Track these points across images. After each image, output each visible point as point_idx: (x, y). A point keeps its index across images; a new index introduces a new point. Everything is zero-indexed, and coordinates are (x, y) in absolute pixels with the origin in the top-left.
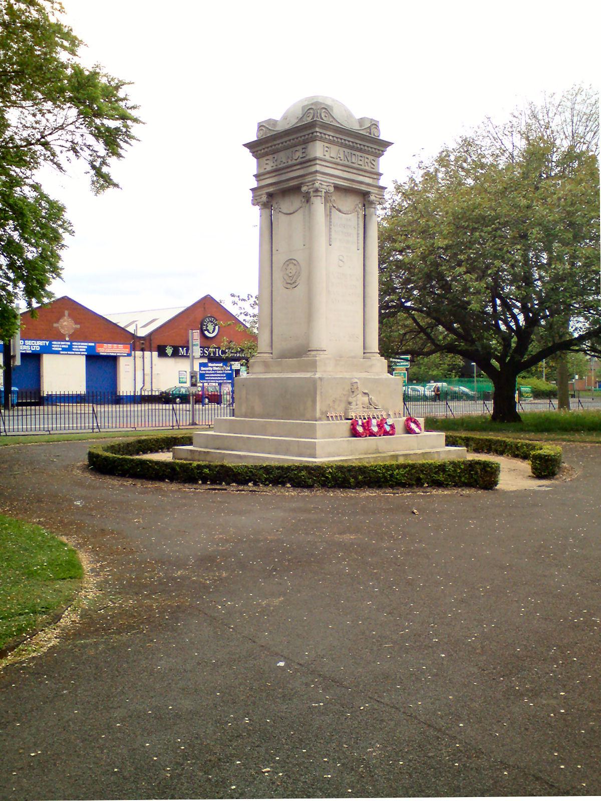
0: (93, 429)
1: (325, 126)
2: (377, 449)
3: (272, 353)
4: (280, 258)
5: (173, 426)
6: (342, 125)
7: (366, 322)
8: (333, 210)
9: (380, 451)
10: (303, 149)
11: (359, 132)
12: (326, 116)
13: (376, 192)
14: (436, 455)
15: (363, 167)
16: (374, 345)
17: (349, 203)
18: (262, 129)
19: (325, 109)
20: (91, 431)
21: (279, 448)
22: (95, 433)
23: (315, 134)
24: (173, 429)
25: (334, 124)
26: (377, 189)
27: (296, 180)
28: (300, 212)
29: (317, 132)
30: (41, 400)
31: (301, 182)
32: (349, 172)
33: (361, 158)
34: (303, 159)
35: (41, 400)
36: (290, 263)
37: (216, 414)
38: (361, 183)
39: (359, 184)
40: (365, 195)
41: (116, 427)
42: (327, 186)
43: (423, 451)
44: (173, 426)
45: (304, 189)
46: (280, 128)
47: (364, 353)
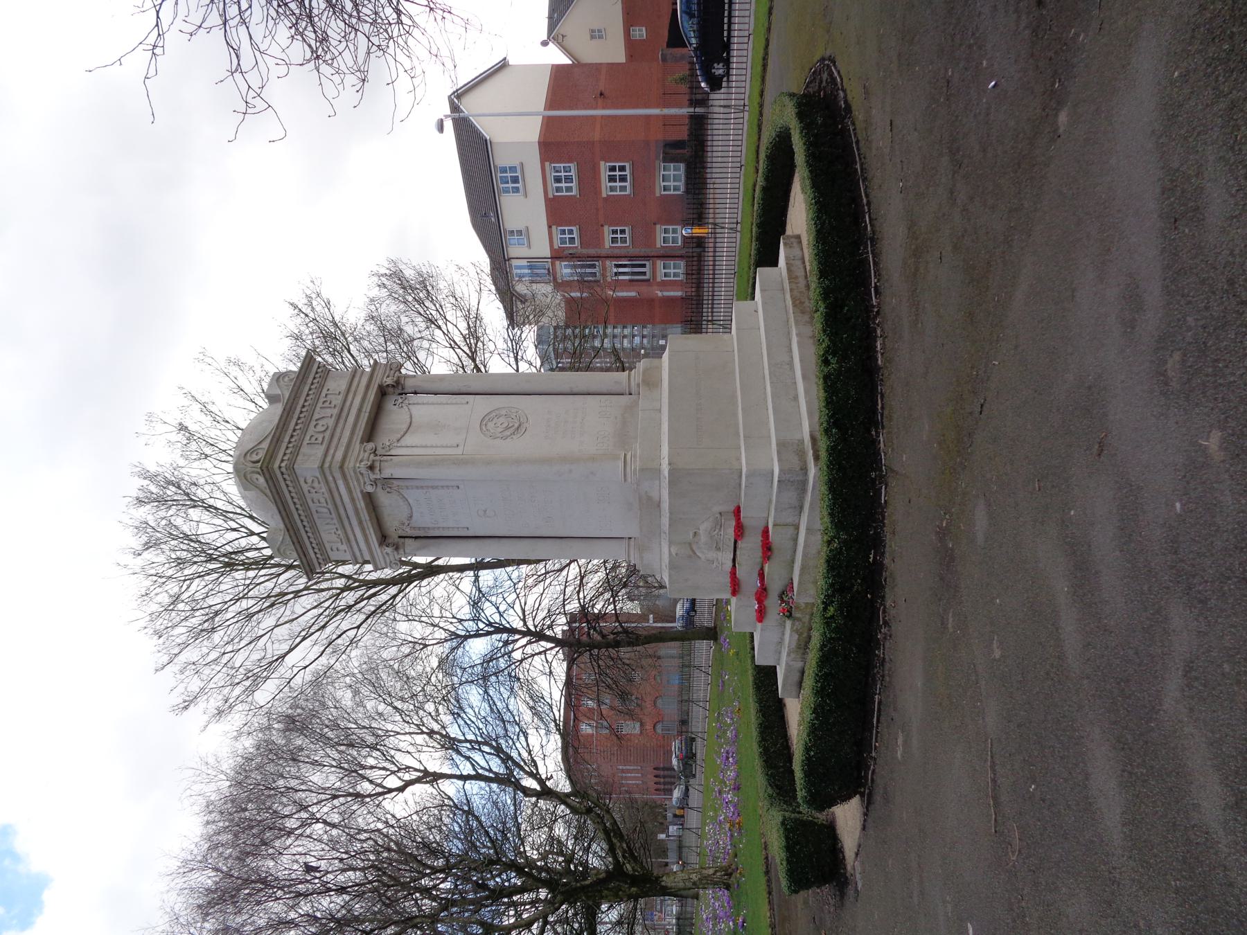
0: (737, 223)
1: (271, 454)
6: (270, 433)
7: (584, 540)
8: (410, 407)
10: (313, 502)
11: (270, 494)
12: (257, 454)
15: (330, 506)
17: (396, 415)
18: (284, 550)
21: (781, 370)
23: (283, 470)
25: (265, 445)
29: (280, 467)
30: (715, 627)
33: (313, 439)
35: (715, 627)
37: (724, 143)
38: (360, 410)
39: (367, 401)
40: (383, 392)
41: (739, 178)
44: (737, 223)
45: (370, 489)
46: (277, 522)
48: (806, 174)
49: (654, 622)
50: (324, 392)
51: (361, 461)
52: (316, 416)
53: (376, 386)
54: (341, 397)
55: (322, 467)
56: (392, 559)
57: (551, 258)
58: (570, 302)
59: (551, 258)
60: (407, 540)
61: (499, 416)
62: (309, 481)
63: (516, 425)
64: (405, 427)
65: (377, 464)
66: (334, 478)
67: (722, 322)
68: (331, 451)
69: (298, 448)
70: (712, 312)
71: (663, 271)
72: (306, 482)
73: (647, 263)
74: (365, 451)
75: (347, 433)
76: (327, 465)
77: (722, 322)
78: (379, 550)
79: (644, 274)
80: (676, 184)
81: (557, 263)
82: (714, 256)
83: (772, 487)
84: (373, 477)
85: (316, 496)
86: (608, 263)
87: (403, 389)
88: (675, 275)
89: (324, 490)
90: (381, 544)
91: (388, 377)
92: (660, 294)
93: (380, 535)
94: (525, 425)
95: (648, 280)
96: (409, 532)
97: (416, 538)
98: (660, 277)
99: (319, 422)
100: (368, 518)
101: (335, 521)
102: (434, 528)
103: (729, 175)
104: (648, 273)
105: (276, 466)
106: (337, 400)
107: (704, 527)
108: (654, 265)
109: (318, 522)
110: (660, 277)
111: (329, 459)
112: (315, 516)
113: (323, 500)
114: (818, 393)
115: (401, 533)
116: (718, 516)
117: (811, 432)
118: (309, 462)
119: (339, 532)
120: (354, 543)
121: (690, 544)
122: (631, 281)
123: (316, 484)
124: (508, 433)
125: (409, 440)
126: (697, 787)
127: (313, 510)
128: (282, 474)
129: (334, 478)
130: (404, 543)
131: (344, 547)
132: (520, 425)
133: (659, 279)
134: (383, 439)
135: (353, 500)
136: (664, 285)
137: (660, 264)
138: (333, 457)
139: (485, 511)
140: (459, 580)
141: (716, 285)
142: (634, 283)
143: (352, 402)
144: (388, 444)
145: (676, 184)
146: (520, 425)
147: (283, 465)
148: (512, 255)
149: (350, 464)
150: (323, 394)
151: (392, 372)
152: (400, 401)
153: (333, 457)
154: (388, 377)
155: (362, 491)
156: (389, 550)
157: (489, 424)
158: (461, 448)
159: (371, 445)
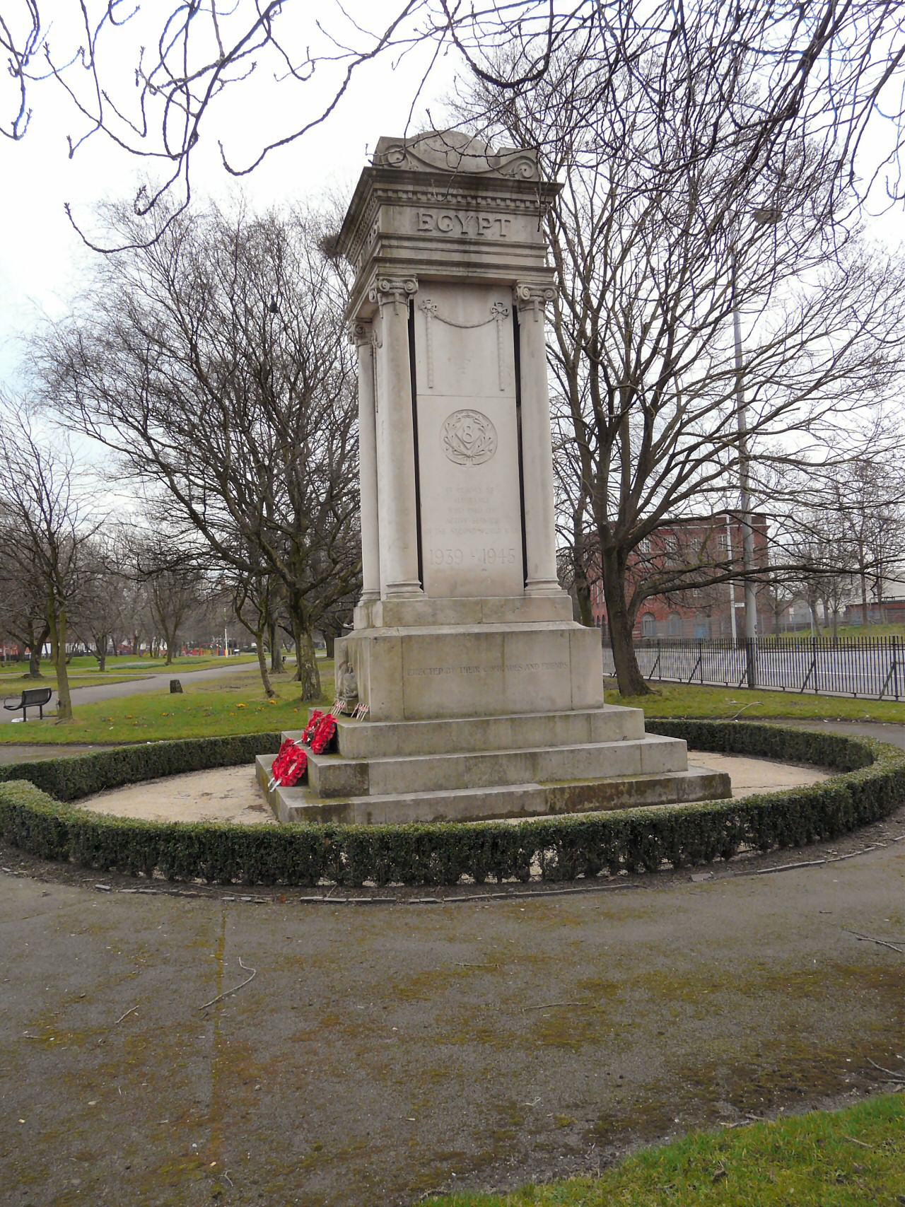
0: (897, 697)
4: (433, 412)
24: (897, 701)
36: (468, 416)
47: (526, 585)
48: (40, 810)
49: (387, 625)
50: (503, 217)
53: (513, 277)
54: (496, 238)
61: (482, 429)
63: (469, 453)
64: (461, 321)
65: (391, 299)
68: (406, 244)
74: (405, 282)
75: (437, 256)
83: (447, 752)
91: (530, 289)
94: (469, 463)
106: (490, 235)
111: (394, 243)
114: (34, 761)
124: (455, 443)
125: (438, 330)
132: (469, 457)
134: (428, 299)
138: (398, 247)
140: (778, 518)
143: (507, 254)
144: (429, 306)
146: (469, 457)
151: (540, 293)
153: (398, 247)
154: (530, 289)
158: (429, 392)
159: (414, 286)
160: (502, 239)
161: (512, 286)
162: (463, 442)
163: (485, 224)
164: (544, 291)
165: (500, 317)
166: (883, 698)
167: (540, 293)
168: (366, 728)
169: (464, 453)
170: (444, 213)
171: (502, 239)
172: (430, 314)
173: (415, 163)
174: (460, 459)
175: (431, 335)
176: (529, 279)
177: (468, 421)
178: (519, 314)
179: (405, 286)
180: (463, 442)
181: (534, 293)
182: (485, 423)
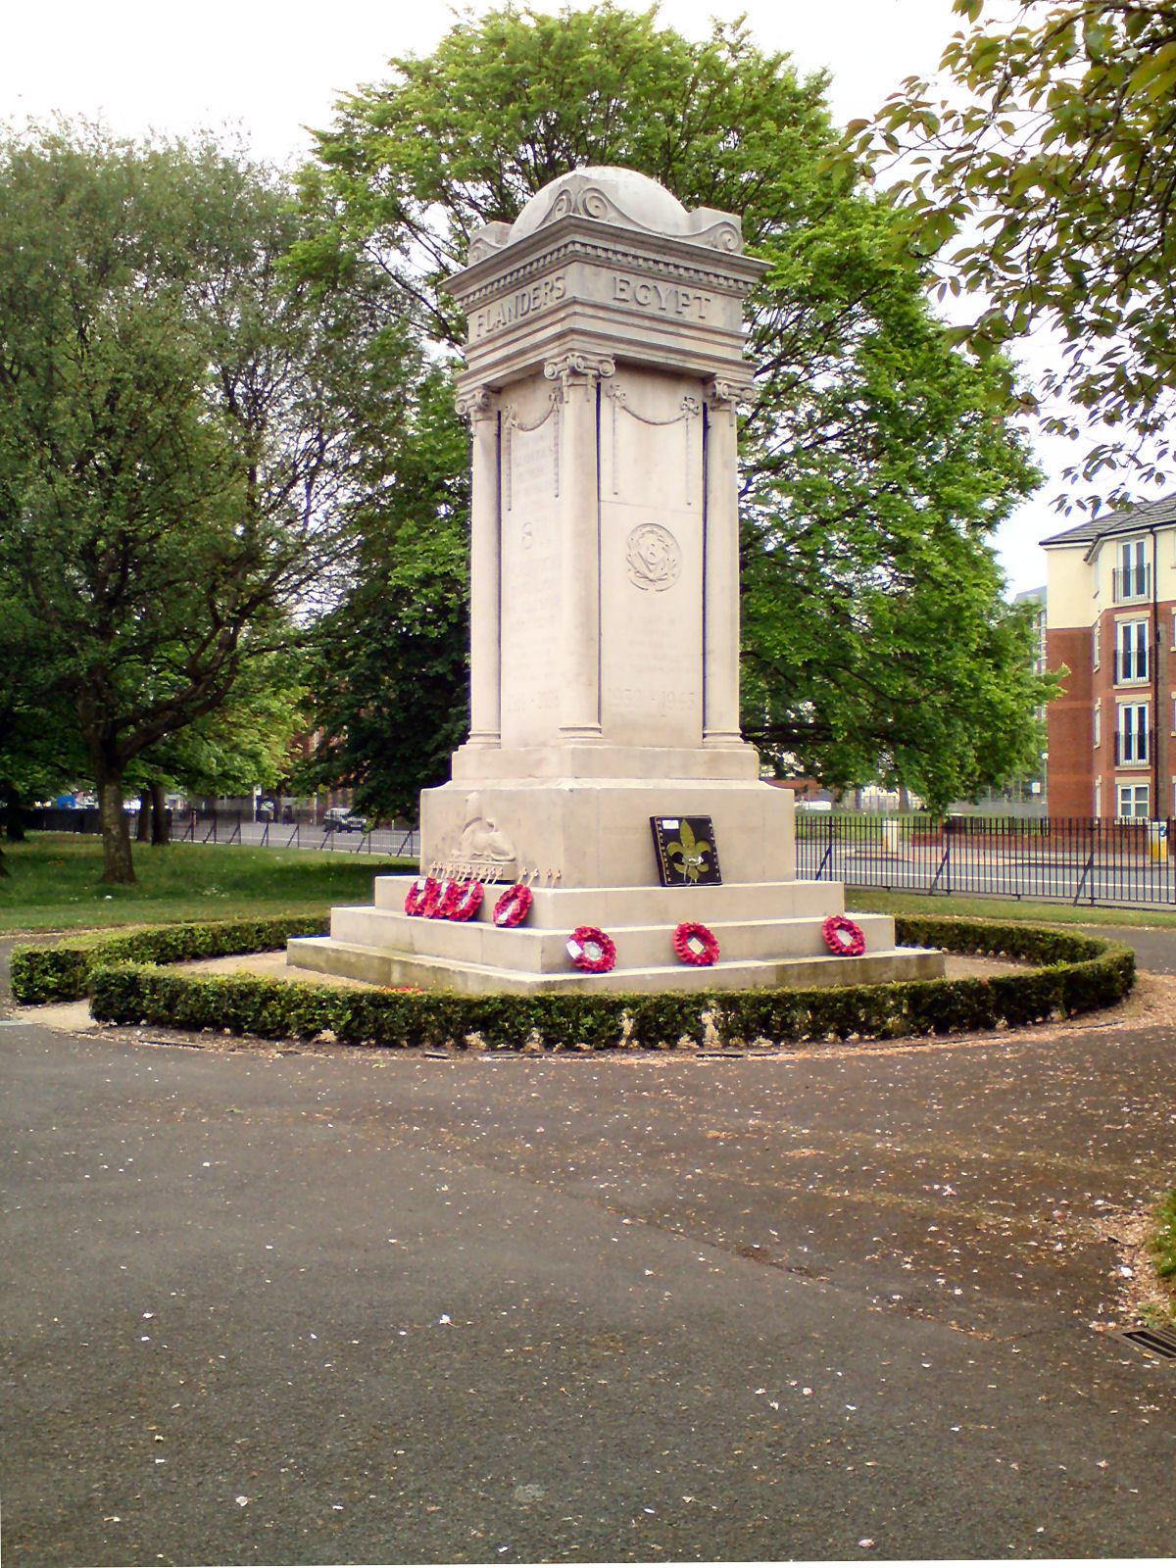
0: (1092, 899)
2: (412, 944)
3: (599, 730)
4: (619, 520)
5: (1092, 899)
9: (417, 949)
13: (556, 351)
14: (459, 980)
15: (531, 314)
16: (728, 713)
19: (596, 190)
20: (1072, 901)
22: (1078, 909)
23: (571, 248)
24: (1092, 905)
26: (556, 344)
27: (662, 354)
28: (680, 426)
29: (574, 243)
31: (540, 358)
32: (627, 324)
33: (623, 286)
34: (640, 308)
36: (652, 532)
42: (601, 362)
43: (439, 962)
45: (548, 371)
47: (704, 736)
51: (584, 358)
52: (661, 286)
53: (713, 371)
55: (575, 302)
56: (469, 403)
57: (1155, 604)
58: (1086, 634)
59: (1155, 604)
60: (495, 422)
62: (559, 284)
63: (651, 576)
64: (649, 416)
65: (582, 381)
66: (563, 319)
67: (1088, 883)
69: (607, 264)
70: (1023, 865)
71: (1133, 789)
72: (558, 279)
73: (1146, 761)
76: (578, 308)
77: (1088, 883)
78: (479, 383)
79: (1128, 756)
80: (1133, 808)
81: (1148, 613)
82: (1136, 869)
84: (564, 375)
85: (541, 293)
86: (1149, 696)
87: (713, 409)
88: (1126, 809)
89: (550, 304)
90: (486, 386)
91: (729, 386)
92: (1098, 782)
93: (499, 384)
94: (652, 588)
95: (1117, 763)
96: (505, 426)
97: (499, 436)
98: (1121, 782)
99: (653, 292)
100: (515, 368)
101: (514, 321)
102: (509, 461)
103: (1125, 885)
104: (1142, 761)
105: (578, 238)
106: (690, 315)
107: (498, 837)
108: (1144, 772)
109: (512, 297)
110: (1121, 782)
112: (518, 293)
113: (538, 302)
115: (504, 414)
116: (511, 857)
117: (448, 970)
118: (576, 281)
119: (501, 327)
120: (490, 347)
121: (479, 819)
122: (1116, 736)
123: (556, 293)
125: (626, 422)
126: (295, 840)
127: (524, 291)
128: (566, 246)
129: (563, 319)
130: (489, 419)
131: (484, 334)
133: (1118, 780)
134: (628, 389)
135: (536, 347)
136: (1111, 790)
137: (1145, 781)
139: (530, 534)
141: (1046, 870)
142: (1112, 740)
144: (618, 393)
145: (1133, 808)
147: (578, 247)
148: (1161, 538)
149: (576, 342)
150: (700, 293)
152: (692, 406)
154: (729, 386)
155: (545, 360)
156: (479, 398)
157: (655, 537)
158: (614, 498)
159: (610, 368)
160: (700, 321)
161: (706, 380)
162: (646, 562)
163: (684, 300)
164: (601, 362)
165: (691, 415)
166: (1079, 901)
167: (738, 392)
168: (906, 960)
169: (648, 576)
170: (643, 281)
171: (700, 321)
172: (618, 403)
173: (613, 214)
174: (642, 583)
175: (620, 429)
176: (729, 374)
177: (651, 539)
178: (710, 414)
179: (601, 367)
180: (646, 562)
181: (590, 364)
182: (669, 541)
